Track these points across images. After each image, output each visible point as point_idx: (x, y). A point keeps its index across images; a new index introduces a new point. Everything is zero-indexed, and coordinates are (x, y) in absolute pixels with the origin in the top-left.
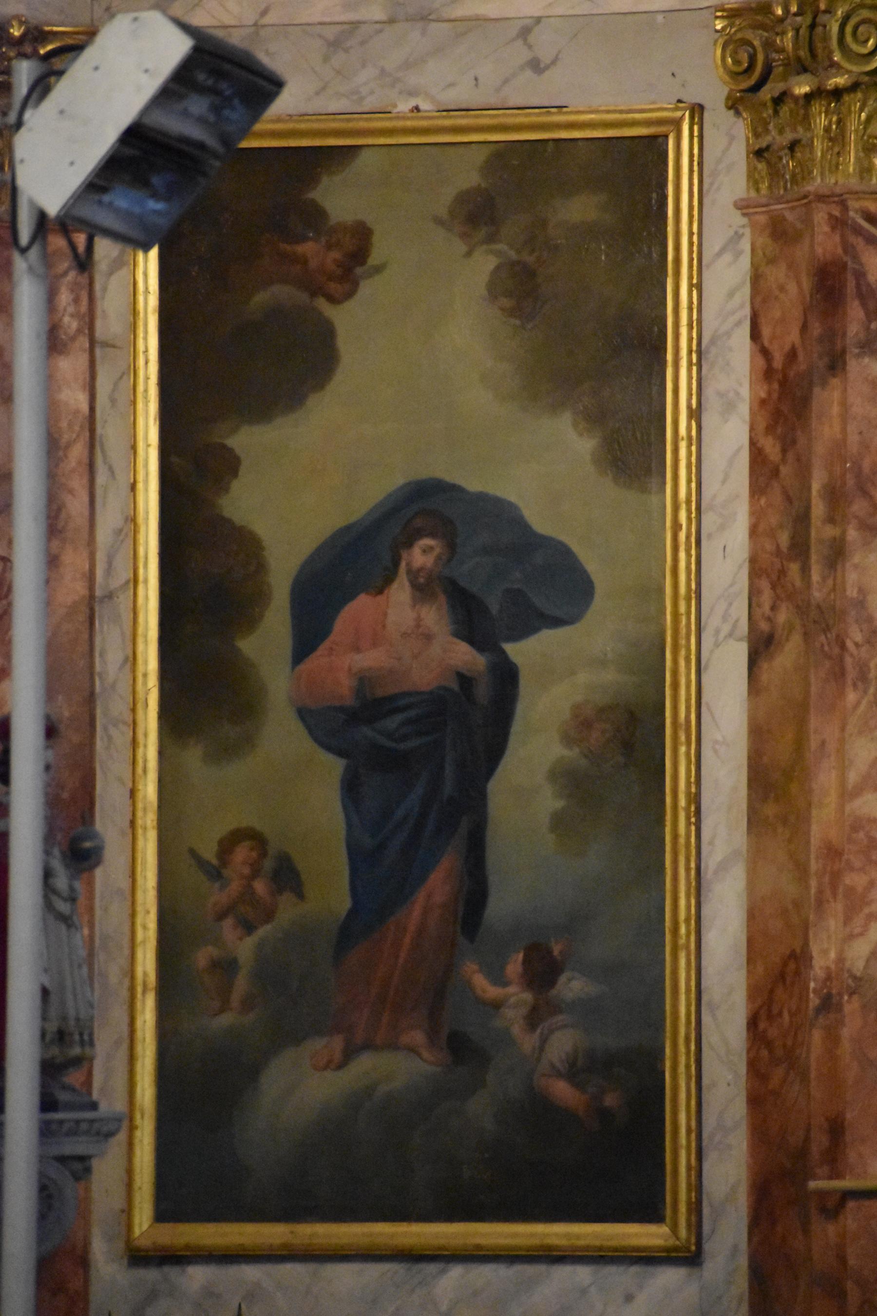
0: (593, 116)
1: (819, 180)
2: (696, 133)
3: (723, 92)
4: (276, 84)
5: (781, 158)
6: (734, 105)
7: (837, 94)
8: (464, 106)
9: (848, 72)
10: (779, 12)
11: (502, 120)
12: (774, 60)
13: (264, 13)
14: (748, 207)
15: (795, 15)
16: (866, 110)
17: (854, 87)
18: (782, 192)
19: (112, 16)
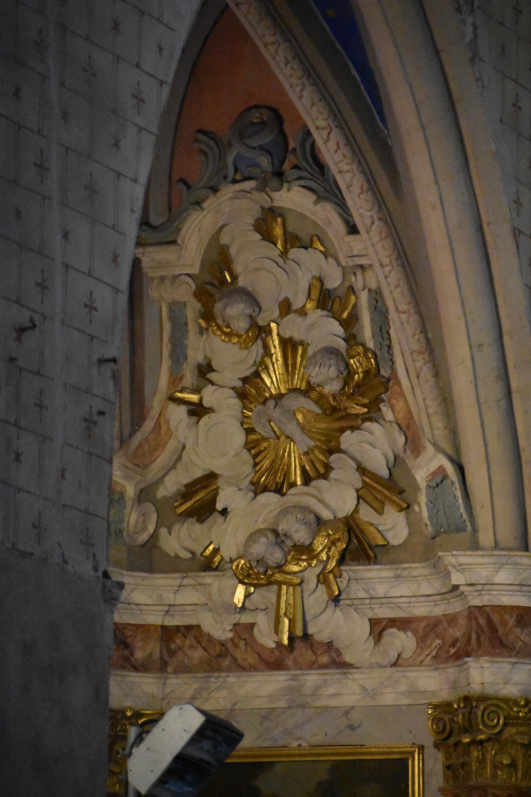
0: (376, 750)
1: (474, 780)
2: (421, 758)
3: (433, 740)
4: (241, 736)
5: (458, 770)
6: (437, 746)
7: (481, 742)
8: (321, 745)
9: (486, 733)
10: (456, 706)
11: (337, 751)
12: (454, 727)
13: (234, 704)
14: (444, 791)
15: (463, 708)
16: (494, 750)
17: (488, 740)
18: (459, 784)
19: (170, 708)
